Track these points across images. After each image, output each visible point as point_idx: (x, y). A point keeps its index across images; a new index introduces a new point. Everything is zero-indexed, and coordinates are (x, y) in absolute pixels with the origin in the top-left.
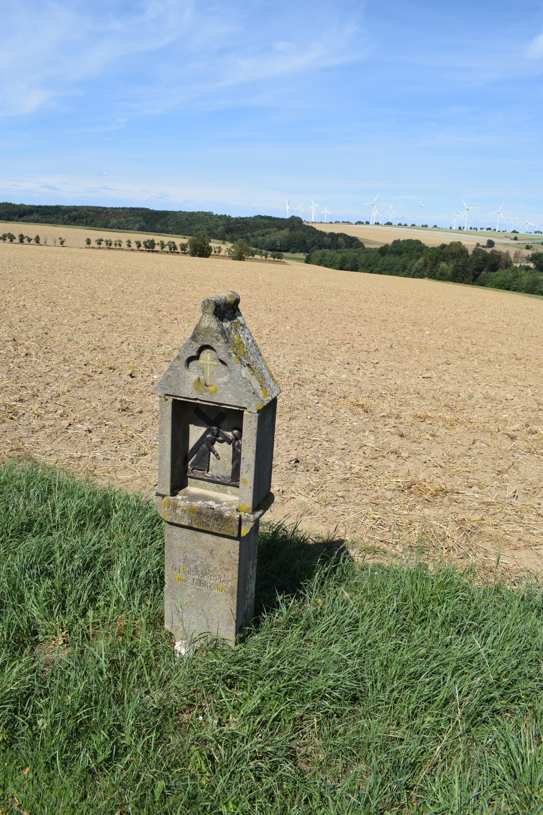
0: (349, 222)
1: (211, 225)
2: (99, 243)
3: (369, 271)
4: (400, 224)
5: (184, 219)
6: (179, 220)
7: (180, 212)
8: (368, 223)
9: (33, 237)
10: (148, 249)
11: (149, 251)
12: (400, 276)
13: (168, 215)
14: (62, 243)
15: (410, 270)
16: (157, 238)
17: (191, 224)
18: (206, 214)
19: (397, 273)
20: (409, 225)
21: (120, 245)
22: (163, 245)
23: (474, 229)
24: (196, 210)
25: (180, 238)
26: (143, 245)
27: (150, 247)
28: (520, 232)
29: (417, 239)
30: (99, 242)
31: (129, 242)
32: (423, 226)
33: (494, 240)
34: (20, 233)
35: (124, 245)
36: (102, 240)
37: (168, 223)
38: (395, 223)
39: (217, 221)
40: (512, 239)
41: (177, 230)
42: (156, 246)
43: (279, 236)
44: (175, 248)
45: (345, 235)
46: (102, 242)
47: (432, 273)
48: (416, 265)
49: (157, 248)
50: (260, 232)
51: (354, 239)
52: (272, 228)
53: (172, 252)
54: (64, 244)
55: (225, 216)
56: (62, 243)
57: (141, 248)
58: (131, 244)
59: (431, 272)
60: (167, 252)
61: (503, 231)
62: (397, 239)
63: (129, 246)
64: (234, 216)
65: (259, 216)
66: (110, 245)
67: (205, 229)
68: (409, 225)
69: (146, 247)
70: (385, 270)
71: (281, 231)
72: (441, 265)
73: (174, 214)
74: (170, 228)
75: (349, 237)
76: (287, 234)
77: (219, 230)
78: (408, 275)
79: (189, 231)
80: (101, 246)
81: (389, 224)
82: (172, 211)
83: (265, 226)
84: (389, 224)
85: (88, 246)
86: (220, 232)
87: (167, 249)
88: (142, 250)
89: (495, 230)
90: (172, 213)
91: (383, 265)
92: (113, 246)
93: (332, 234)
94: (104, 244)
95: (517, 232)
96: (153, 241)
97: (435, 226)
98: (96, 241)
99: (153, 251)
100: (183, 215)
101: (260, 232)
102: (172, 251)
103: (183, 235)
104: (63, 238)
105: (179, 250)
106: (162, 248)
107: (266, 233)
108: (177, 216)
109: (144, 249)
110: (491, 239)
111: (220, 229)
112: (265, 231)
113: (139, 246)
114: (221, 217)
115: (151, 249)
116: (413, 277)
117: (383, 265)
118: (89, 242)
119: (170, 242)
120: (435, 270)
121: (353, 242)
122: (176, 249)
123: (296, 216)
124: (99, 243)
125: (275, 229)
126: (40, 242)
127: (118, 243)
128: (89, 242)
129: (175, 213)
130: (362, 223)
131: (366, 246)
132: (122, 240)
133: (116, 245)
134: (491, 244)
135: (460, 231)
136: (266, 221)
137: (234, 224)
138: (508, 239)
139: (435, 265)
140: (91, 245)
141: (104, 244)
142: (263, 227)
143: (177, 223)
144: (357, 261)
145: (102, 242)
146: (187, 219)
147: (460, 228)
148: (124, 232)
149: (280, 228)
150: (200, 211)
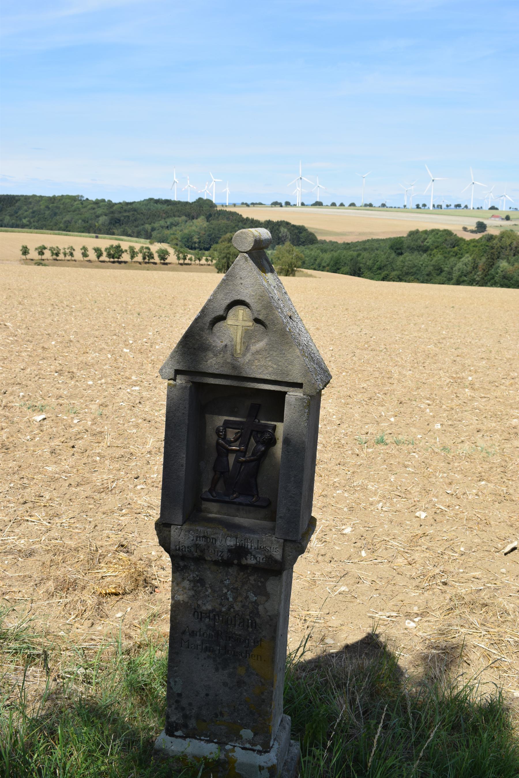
0: (260, 204)
1: (87, 215)
2: (41, 253)
3: (381, 277)
5: (43, 207)
6: (35, 209)
7: (34, 196)
10: (112, 260)
11: (114, 262)
12: (435, 283)
13: (17, 201)
15: (450, 273)
16: (126, 243)
17: (55, 214)
18: (74, 199)
19: (428, 279)
20: (347, 204)
21: (71, 254)
22: (133, 253)
23: (438, 206)
24: (58, 194)
25: (91, 237)
26: (105, 254)
27: (116, 255)
28: (500, 209)
30: (41, 251)
31: (85, 249)
32: (366, 205)
33: (486, 222)
35: (78, 255)
36: (45, 248)
37: (20, 212)
38: (327, 202)
39: (94, 209)
40: (503, 219)
41: (36, 224)
42: (123, 255)
43: (194, 228)
44: (151, 256)
45: (288, 223)
46: (45, 251)
47: (489, 277)
48: (460, 265)
49: (126, 257)
50: (162, 223)
51: (301, 229)
52: (179, 216)
53: (146, 263)
55: (103, 201)
57: (101, 259)
58: (88, 253)
59: (486, 276)
60: (140, 263)
61: (478, 208)
62: (414, 229)
63: (85, 255)
64: (115, 200)
65: (151, 200)
66: (57, 254)
67: (80, 221)
68: (347, 204)
69: (109, 255)
70: (407, 274)
71: (195, 221)
72: (501, 265)
73: (26, 200)
74: (25, 221)
75: (294, 226)
76: (205, 225)
78: (448, 280)
79: (56, 224)
80: (44, 257)
81: (318, 204)
82: (22, 196)
83: (168, 215)
84: (318, 204)
85: (24, 257)
86: (103, 225)
87: (139, 258)
88: (103, 262)
89: (466, 207)
90: (23, 198)
91: (403, 267)
92: (61, 256)
94: (47, 254)
95: (497, 209)
96: (118, 247)
97: (383, 205)
98: (36, 249)
99: (120, 262)
100: (39, 201)
101: (162, 223)
102: (147, 260)
103: (95, 233)
105: (157, 259)
106: (132, 257)
107: (172, 225)
108: (30, 203)
109: (107, 259)
110: (481, 220)
111: (103, 219)
112: (169, 221)
113: (99, 254)
114: (97, 203)
115: (116, 260)
116: (458, 283)
117: (403, 267)
118: (25, 251)
119: (142, 247)
120: (492, 271)
121: (300, 233)
122: (153, 258)
123: (205, 198)
124: (41, 253)
125: (184, 218)
127: (68, 251)
128: (25, 251)
131: (319, 238)
132: (75, 248)
133: (65, 254)
134: (481, 227)
135: (418, 210)
137: (120, 212)
138: (497, 219)
139: (491, 266)
140: (29, 256)
141: (47, 254)
142: (164, 215)
143: (33, 212)
144: (360, 263)
145: (45, 251)
146: (47, 207)
147: (418, 207)
148: (6, 231)
149: (192, 217)
150: (65, 194)
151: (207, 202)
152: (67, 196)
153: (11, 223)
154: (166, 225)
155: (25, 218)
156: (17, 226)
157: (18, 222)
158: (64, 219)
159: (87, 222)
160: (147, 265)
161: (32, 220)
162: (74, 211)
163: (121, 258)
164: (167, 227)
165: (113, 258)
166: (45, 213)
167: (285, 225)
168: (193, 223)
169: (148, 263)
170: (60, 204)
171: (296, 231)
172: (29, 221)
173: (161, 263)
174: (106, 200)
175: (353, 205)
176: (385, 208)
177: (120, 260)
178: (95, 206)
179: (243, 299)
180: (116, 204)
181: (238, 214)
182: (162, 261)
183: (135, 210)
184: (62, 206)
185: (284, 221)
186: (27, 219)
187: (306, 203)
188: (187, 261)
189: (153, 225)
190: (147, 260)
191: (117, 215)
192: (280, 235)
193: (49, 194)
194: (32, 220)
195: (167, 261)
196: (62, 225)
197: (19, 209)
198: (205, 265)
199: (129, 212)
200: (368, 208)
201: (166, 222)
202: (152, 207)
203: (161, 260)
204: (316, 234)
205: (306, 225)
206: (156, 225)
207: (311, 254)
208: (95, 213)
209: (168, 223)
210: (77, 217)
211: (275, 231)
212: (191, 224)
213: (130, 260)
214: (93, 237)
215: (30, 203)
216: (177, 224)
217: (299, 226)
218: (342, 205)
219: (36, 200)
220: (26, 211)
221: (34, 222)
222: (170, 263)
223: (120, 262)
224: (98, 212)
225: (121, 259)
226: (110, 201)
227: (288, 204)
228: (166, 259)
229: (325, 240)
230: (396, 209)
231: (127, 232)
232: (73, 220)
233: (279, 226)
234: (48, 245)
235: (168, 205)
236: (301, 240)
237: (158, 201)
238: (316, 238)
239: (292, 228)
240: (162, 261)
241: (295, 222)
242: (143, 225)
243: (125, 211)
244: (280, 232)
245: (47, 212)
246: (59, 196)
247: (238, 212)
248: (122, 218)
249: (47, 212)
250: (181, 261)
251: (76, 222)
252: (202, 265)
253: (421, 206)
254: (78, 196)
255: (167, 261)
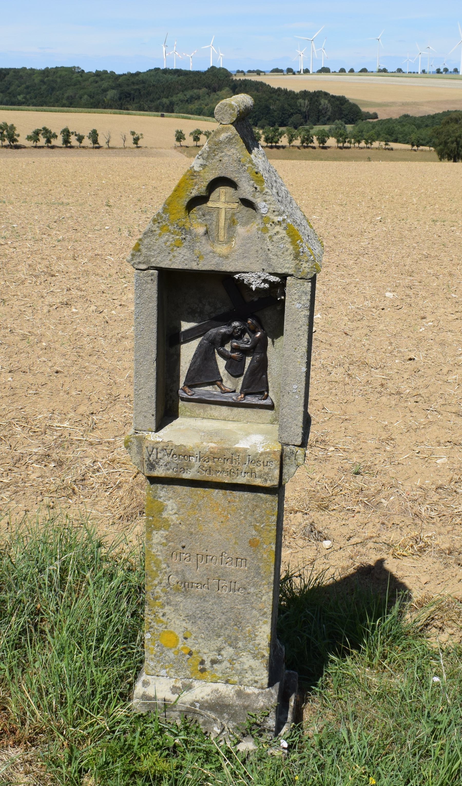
2: (196, 139)
4: (342, 70)
7: (24, 69)
8: (307, 71)
9: (86, 133)
10: (269, 144)
13: (5, 75)
14: (136, 141)
18: (71, 71)
25: (155, 116)
29: (303, 89)
32: (380, 71)
34: (64, 127)
36: (200, 133)
38: (334, 68)
39: (97, 82)
50: (181, 96)
53: (305, 147)
54: (140, 143)
55: (105, 72)
56: (136, 141)
60: (298, 148)
64: (118, 72)
71: (218, 93)
74: (20, 98)
75: (333, 97)
77: (108, 97)
81: (325, 70)
84: (325, 70)
85: (178, 144)
93: (305, 94)
97: (400, 70)
98: (191, 134)
99: (278, 147)
104: (138, 132)
111: (111, 94)
112: (189, 93)
114: (98, 74)
121: (342, 104)
122: (312, 141)
124: (196, 139)
125: (204, 90)
126: (99, 141)
128: (180, 137)
129: (16, 71)
130: (281, 71)
131: (364, 109)
135: (439, 75)
136: (175, 78)
140: (183, 143)
146: (42, 81)
150: (59, 66)
151: (222, 71)
152: (61, 67)
153: (5, 100)
154: (186, 99)
155: (19, 95)
156: (13, 104)
157: (14, 100)
158: (66, 95)
159: (93, 97)
160: (307, 150)
161: (28, 97)
162: (75, 85)
163: (280, 142)
164: (187, 101)
165: (271, 143)
166: (41, 88)
167: (323, 95)
168: (218, 95)
169: (307, 147)
170: (56, 77)
171: (338, 102)
172: (25, 98)
173: (320, 147)
174: (109, 72)
175: (364, 70)
176: (401, 74)
177: (277, 144)
178: (98, 79)
179: (228, 176)
180: (120, 76)
181: (265, 84)
182: (321, 145)
183: (143, 82)
184: (59, 80)
185: (321, 91)
186: (22, 96)
187: (295, 70)
188: (346, 144)
189: (170, 98)
190: (305, 144)
191: (126, 89)
192: (320, 107)
193: (40, 66)
194: (28, 97)
195: (326, 145)
196: (64, 102)
197: (10, 84)
198: (364, 148)
199: (137, 84)
200: (383, 74)
201: (185, 95)
202: (161, 78)
203: (320, 143)
204: (359, 106)
205: (347, 96)
206: (174, 99)
207: (404, 130)
208: (100, 87)
209: (188, 96)
210: (81, 92)
211: (314, 103)
212: (216, 97)
213: (288, 144)
214: (157, 116)
215: (21, 77)
216: (198, 98)
217: (339, 97)
218: (352, 71)
219: (27, 73)
220: (19, 87)
221: (31, 98)
222: (329, 147)
223: (278, 147)
224: (103, 86)
225: (280, 144)
226: (112, 73)
227: (290, 71)
228: (326, 142)
229: (368, 113)
230: (413, 74)
231: (144, 108)
232: (77, 97)
233: (318, 97)
234: (203, 130)
235: (179, 76)
236: (344, 112)
237: (166, 71)
238: (360, 110)
239: (333, 99)
240: (321, 145)
241: (334, 92)
242: (159, 99)
243: (133, 83)
244: (320, 104)
245: (44, 87)
246: (53, 68)
247: (264, 81)
248: (132, 92)
249: (44, 87)
250: (341, 145)
251: (81, 98)
252: (362, 148)
253: (442, 70)
254: (74, 67)
255: (326, 145)
